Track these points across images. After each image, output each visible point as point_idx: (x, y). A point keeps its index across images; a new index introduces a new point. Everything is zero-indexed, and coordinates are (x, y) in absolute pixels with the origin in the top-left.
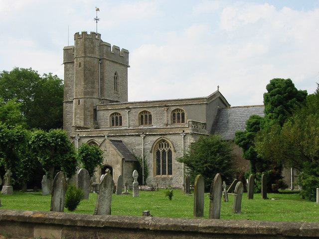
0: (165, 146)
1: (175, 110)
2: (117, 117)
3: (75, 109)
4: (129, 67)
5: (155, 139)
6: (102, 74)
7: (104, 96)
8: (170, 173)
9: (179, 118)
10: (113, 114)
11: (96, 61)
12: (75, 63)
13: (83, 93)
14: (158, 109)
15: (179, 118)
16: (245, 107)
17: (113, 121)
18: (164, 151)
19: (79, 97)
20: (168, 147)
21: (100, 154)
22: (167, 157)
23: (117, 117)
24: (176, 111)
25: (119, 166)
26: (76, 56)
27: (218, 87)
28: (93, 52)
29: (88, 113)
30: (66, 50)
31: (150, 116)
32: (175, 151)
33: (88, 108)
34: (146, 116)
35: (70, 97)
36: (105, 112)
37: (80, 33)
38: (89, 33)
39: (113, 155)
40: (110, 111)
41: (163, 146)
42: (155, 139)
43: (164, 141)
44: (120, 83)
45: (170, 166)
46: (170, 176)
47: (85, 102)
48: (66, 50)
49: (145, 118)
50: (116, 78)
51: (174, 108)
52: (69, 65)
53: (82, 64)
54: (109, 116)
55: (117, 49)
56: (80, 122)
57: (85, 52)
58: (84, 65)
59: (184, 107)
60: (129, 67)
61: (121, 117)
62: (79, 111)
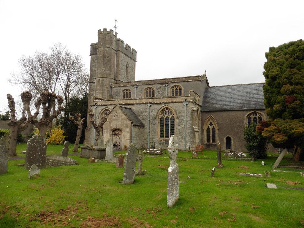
0: (169, 114)
1: (173, 87)
2: (127, 93)
5: (158, 107)
6: (117, 61)
7: (118, 78)
9: (177, 93)
10: (124, 90)
11: (113, 51)
14: (160, 85)
15: (177, 93)
16: (227, 86)
17: (124, 95)
18: (167, 118)
19: (100, 77)
20: (171, 114)
23: (127, 93)
24: (175, 87)
25: (128, 130)
27: (205, 71)
28: (111, 44)
29: (106, 89)
30: (92, 45)
31: (153, 91)
32: (178, 118)
34: (150, 91)
36: (119, 88)
37: (102, 30)
39: (123, 119)
40: (122, 88)
41: (166, 114)
42: (158, 107)
43: (167, 109)
44: (130, 69)
48: (92, 45)
49: (150, 93)
50: (127, 67)
52: (94, 56)
54: (121, 91)
55: (128, 46)
56: (99, 96)
60: (137, 62)
61: (130, 92)
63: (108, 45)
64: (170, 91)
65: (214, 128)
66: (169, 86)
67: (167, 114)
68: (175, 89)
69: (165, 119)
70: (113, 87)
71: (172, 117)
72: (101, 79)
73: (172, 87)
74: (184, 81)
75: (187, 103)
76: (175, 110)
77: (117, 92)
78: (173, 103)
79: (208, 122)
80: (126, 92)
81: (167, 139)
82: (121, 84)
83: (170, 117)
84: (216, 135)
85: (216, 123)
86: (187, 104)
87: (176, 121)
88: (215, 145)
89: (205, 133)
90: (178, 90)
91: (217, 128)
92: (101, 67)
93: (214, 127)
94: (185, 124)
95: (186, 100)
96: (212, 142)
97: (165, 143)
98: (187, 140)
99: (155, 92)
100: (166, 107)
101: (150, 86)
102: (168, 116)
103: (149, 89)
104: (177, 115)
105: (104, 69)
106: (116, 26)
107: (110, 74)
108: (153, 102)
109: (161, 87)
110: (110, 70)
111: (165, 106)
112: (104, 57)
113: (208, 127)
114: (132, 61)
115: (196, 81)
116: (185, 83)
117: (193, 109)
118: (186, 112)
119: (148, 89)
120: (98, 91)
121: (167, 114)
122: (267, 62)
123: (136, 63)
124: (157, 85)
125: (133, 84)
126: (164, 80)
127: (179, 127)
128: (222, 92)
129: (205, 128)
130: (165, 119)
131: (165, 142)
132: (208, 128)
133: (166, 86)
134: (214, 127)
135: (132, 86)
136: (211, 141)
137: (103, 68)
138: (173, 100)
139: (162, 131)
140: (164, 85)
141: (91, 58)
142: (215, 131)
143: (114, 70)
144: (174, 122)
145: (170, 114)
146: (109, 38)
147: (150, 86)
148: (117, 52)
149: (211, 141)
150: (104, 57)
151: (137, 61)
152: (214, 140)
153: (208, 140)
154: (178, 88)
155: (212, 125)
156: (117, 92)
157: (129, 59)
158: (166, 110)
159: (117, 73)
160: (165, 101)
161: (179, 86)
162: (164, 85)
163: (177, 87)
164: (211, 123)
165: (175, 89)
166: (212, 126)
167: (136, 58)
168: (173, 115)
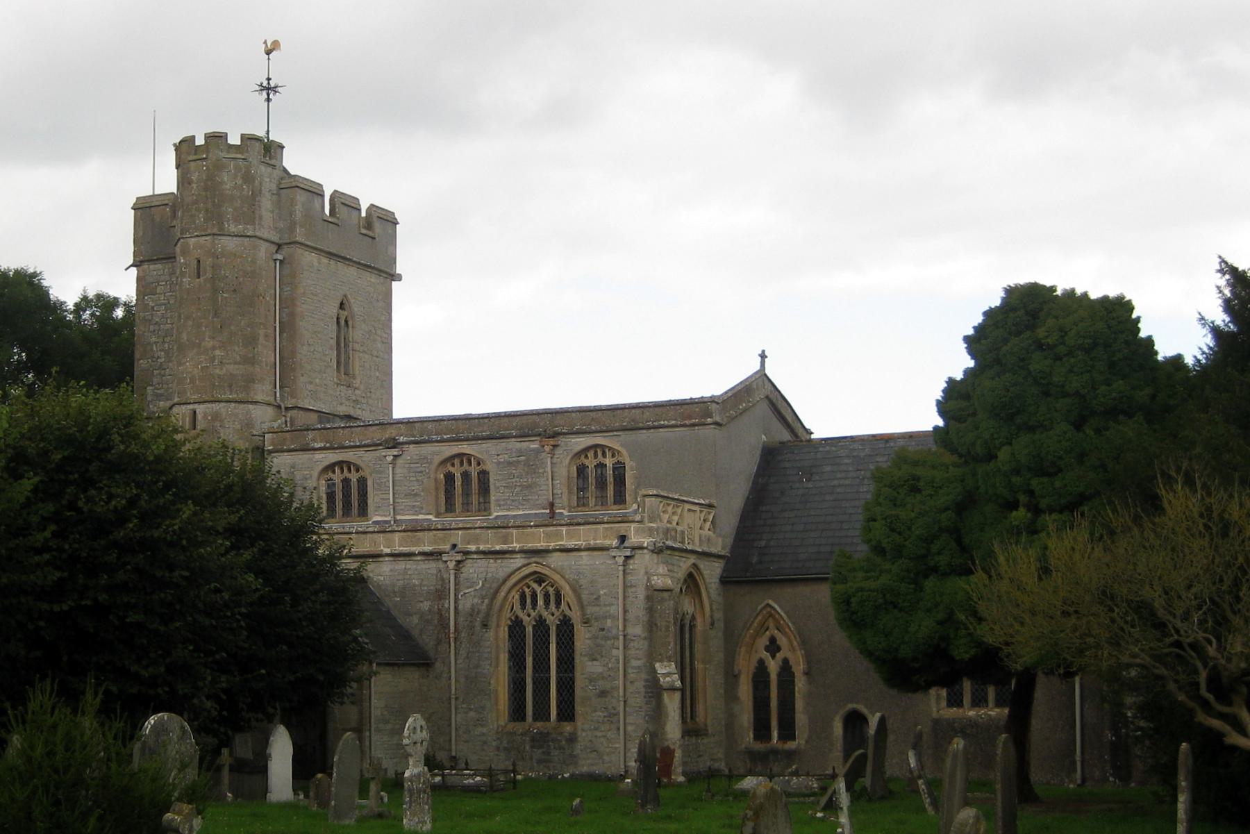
0: (547, 602)
2: (346, 482)
6: (288, 303)
7: (293, 395)
8: (567, 713)
9: (601, 484)
10: (330, 468)
11: (263, 250)
14: (514, 444)
15: (601, 484)
18: (541, 624)
23: (346, 482)
24: (591, 454)
30: (146, 210)
31: (484, 475)
34: (466, 476)
35: (159, 397)
37: (200, 141)
40: (318, 456)
43: (540, 579)
46: (568, 727)
50: (343, 324)
52: (156, 269)
54: (315, 474)
61: (362, 482)
63: (237, 220)
64: (565, 473)
65: (786, 668)
66: (558, 451)
67: (541, 602)
69: (529, 630)
70: (270, 452)
72: (200, 409)
73: (579, 454)
75: (628, 554)
76: (574, 590)
79: (758, 634)
80: (337, 477)
81: (539, 724)
82: (311, 435)
84: (799, 704)
85: (795, 643)
86: (627, 558)
87: (582, 639)
88: (790, 755)
89: (745, 690)
90: (609, 472)
91: (799, 668)
93: (786, 661)
94: (619, 653)
96: (780, 738)
97: (532, 747)
98: (629, 728)
100: (535, 572)
101: (464, 448)
102: (545, 614)
103: (462, 464)
105: (218, 352)
106: (272, 84)
107: (250, 380)
109: (520, 453)
110: (250, 361)
112: (215, 291)
113: (761, 662)
114: (372, 278)
115: (694, 425)
116: (643, 435)
117: (658, 581)
118: (625, 598)
119: (457, 462)
121: (541, 602)
122: (971, 363)
123: (394, 284)
124: (503, 444)
125: (377, 435)
127: (596, 668)
128: (843, 475)
129: (745, 668)
130: (529, 630)
131: (533, 740)
132: (761, 669)
133: (547, 448)
134: (786, 661)
136: (775, 734)
137: (214, 348)
139: (517, 687)
140: (535, 446)
141: (139, 280)
142: (792, 683)
143: (268, 354)
145: (553, 606)
146: (239, 182)
147: (464, 448)
148: (286, 250)
149: (775, 734)
150: (215, 291)
151: (398, 271)
152: (788, 731)
153: (761, 729)
154: (609, 462)
155: (779, 649)
157: (352, 271)
158: (535, 586)
159: (288, 369)
162: (535, 446)
163: (604, 455)
164: (773, 640)
165: (591, 462)
166: (779, 656)
167: (393, 261)
168: (568, 613)
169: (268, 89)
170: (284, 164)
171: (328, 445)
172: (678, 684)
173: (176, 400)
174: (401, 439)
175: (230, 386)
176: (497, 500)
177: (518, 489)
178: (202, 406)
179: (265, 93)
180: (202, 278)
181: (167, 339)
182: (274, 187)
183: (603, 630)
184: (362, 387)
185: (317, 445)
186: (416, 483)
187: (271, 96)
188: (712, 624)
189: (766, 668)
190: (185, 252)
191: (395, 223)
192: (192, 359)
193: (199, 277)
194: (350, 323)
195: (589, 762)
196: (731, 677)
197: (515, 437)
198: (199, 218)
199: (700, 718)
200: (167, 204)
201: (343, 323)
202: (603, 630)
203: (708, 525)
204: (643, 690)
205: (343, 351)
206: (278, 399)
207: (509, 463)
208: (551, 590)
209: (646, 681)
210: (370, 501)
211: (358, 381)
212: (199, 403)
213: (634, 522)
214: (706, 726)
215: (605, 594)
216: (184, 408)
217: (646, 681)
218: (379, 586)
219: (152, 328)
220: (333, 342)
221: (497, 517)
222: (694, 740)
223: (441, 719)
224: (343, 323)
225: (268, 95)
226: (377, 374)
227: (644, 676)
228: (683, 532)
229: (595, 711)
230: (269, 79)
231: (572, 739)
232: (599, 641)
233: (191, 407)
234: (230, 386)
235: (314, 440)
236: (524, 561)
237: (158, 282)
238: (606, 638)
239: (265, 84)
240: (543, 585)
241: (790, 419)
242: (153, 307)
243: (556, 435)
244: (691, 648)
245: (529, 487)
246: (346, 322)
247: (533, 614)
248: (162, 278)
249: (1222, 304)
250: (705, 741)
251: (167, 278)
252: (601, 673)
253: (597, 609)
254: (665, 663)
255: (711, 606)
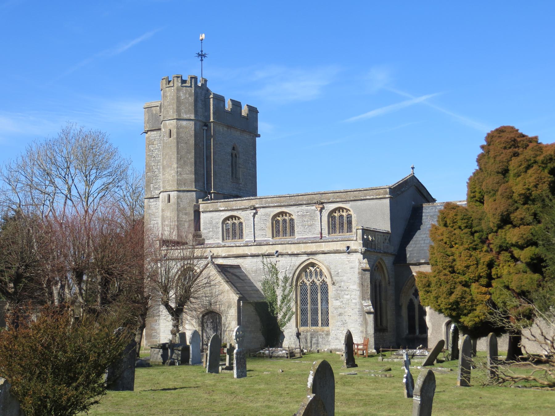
0: (316, 275)
1: (334, 211)
2: (285, 221)
3: (163, 210)
4: (259, 136)
8: (326, 323)
9: (342, 225)
12: (163, 130)
13: (175, 183)
14: (304, 207)
15: (342, 225)
19: (169, 189)
21: (431, 231)
22: (319, 295)
26: (164, 117)
31: (292, 220)
33: (185, 209)
35: (156, 189)
38: (485, 143)
43: (313, 265)
45: (326, 313)
46: (326, 328)
47: (178, 197)
50: (234, 156)
51: (331, 207)
53: (174, 131)
57: (178, 111)
58: (178, 133)
59: (240, 212)
60: (259, 136)
61: (241, 224)
62: (168, 214)
68: (337, 215)
69: (309, 288)
71: (324, 283)
72: (172, 194)
74: (356, 199)
77: (211, 223)
78: (324, 253)
83: (318, 283)
89: (404, 312)
90: (345, 219)
92: (171, 167)
95: (348, 247)
99: (295, 221)
102: (316, 280)
104: (331, 277)
108: (284, 252)
111: (309, 259)
116: (359, 203)
120: (167, 223)
123: (257, 139)
124: (300, 208)
126: (314, 196)
127: (337, 303)
130: (309, 288)
135: (244, 209)
136: (417, 331)
138: (325, 247)
144: (327, 292)
145: (319, 277)
146: (187, 96)
149: (417, 331)
156: (211, 223)
160: (309, 250)
161: (345, 209)
169: (202, 55)
170: (207, 86)
171: (226, 209)
172: (372, 310)
173: (162, 190)
174: (257, 206)
175: (184, 184)
176: (297, 232)
177: (306, 226)
178: (173, 193)
179: (200, 57)
180: (172, 138)
181: (159, 164)
182: (203, 98)
183: (340, 287)
184: (243, 183)
185: (221, 209)
186: (264, 225)
187: (203, 58)
188: (389, 283)
189: (413, 303)
190: (165, 126)
191: (257, 112)
192: (168, 172)
193: (170, 137)
194: (237, 156)
195: (335, 344)
196: (398, 307)
197: (305, 204)
198: (171, 112)
199: (384, 324)
200: (158, 106)
201: (234, 156)
202: (340, 287)
203: (387, 241)
204: (358, 313)
205: (234, 167)
206: (206, 189)
207: (303, 216)
208: (318, 270)
209: (359, 309)
210: (244, 232)
211: (241, 181)
212: (171, 191)
213: (352, 240)
214: (387, 327)
215: (341, 272)
216: (189, 195)
217: (359, 309)
218: (246, 269)
219: (152, 159)
220: (230, 164)
221: (298, 239)
222: (381, 334)
223: (480, 219)
224: (234, 156)
225: (202, 58)
226: (250, 177)
227: (358, 307)
228: (375, 244)
229: (337, 322)
230: (202, 51)
231: (328, 334)
232: (339, 292)
233: (168, 193)
234: (184, 184)
235: (220, 207)
236: (307, 258)
237: (155, 139)
238: (342, 291)
239: (200, 53)
240: (315, 268)
241: (425, 194)
242: (152, 150)
243: (322, 203)
244: (380, 294)
245: (311, 225)
246: (236, 155)
247: (311, 281)
248: (157, 138)
249: (358, 289)
250: (387, 334)
251: (159, 138)
252: (340, 306)
253: (338, 278)
254: (367, 301)
255: (388, 276)
